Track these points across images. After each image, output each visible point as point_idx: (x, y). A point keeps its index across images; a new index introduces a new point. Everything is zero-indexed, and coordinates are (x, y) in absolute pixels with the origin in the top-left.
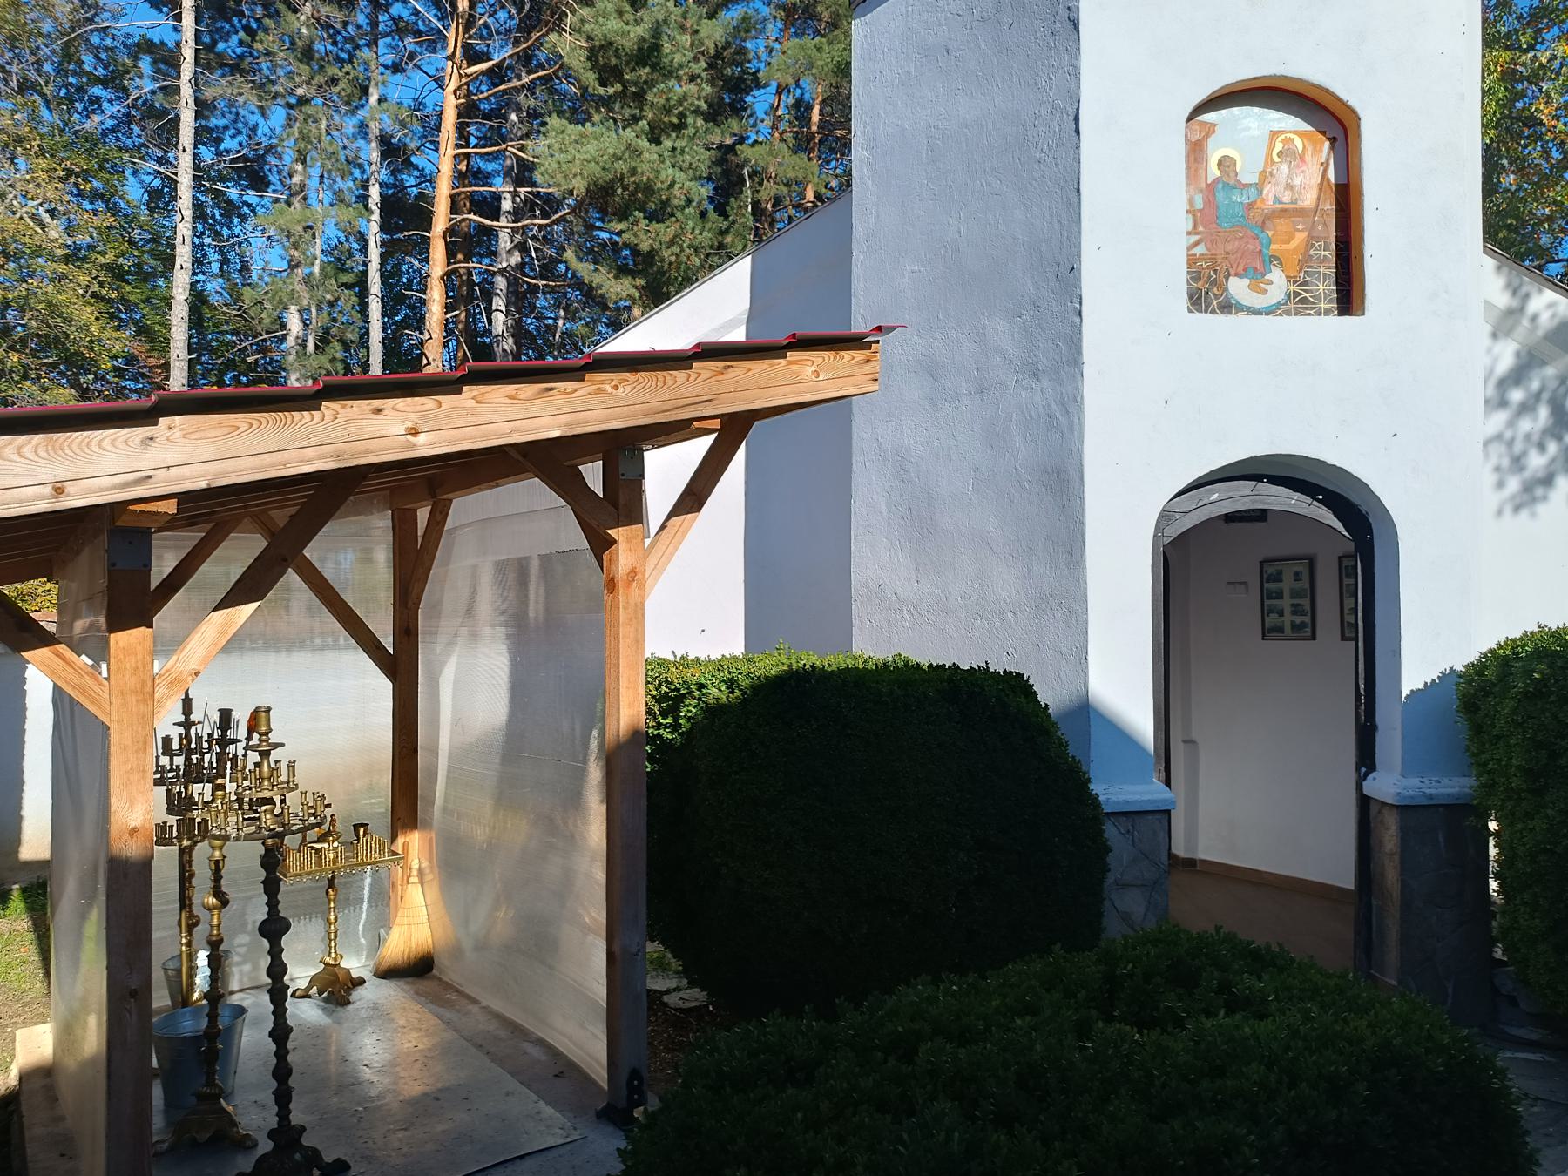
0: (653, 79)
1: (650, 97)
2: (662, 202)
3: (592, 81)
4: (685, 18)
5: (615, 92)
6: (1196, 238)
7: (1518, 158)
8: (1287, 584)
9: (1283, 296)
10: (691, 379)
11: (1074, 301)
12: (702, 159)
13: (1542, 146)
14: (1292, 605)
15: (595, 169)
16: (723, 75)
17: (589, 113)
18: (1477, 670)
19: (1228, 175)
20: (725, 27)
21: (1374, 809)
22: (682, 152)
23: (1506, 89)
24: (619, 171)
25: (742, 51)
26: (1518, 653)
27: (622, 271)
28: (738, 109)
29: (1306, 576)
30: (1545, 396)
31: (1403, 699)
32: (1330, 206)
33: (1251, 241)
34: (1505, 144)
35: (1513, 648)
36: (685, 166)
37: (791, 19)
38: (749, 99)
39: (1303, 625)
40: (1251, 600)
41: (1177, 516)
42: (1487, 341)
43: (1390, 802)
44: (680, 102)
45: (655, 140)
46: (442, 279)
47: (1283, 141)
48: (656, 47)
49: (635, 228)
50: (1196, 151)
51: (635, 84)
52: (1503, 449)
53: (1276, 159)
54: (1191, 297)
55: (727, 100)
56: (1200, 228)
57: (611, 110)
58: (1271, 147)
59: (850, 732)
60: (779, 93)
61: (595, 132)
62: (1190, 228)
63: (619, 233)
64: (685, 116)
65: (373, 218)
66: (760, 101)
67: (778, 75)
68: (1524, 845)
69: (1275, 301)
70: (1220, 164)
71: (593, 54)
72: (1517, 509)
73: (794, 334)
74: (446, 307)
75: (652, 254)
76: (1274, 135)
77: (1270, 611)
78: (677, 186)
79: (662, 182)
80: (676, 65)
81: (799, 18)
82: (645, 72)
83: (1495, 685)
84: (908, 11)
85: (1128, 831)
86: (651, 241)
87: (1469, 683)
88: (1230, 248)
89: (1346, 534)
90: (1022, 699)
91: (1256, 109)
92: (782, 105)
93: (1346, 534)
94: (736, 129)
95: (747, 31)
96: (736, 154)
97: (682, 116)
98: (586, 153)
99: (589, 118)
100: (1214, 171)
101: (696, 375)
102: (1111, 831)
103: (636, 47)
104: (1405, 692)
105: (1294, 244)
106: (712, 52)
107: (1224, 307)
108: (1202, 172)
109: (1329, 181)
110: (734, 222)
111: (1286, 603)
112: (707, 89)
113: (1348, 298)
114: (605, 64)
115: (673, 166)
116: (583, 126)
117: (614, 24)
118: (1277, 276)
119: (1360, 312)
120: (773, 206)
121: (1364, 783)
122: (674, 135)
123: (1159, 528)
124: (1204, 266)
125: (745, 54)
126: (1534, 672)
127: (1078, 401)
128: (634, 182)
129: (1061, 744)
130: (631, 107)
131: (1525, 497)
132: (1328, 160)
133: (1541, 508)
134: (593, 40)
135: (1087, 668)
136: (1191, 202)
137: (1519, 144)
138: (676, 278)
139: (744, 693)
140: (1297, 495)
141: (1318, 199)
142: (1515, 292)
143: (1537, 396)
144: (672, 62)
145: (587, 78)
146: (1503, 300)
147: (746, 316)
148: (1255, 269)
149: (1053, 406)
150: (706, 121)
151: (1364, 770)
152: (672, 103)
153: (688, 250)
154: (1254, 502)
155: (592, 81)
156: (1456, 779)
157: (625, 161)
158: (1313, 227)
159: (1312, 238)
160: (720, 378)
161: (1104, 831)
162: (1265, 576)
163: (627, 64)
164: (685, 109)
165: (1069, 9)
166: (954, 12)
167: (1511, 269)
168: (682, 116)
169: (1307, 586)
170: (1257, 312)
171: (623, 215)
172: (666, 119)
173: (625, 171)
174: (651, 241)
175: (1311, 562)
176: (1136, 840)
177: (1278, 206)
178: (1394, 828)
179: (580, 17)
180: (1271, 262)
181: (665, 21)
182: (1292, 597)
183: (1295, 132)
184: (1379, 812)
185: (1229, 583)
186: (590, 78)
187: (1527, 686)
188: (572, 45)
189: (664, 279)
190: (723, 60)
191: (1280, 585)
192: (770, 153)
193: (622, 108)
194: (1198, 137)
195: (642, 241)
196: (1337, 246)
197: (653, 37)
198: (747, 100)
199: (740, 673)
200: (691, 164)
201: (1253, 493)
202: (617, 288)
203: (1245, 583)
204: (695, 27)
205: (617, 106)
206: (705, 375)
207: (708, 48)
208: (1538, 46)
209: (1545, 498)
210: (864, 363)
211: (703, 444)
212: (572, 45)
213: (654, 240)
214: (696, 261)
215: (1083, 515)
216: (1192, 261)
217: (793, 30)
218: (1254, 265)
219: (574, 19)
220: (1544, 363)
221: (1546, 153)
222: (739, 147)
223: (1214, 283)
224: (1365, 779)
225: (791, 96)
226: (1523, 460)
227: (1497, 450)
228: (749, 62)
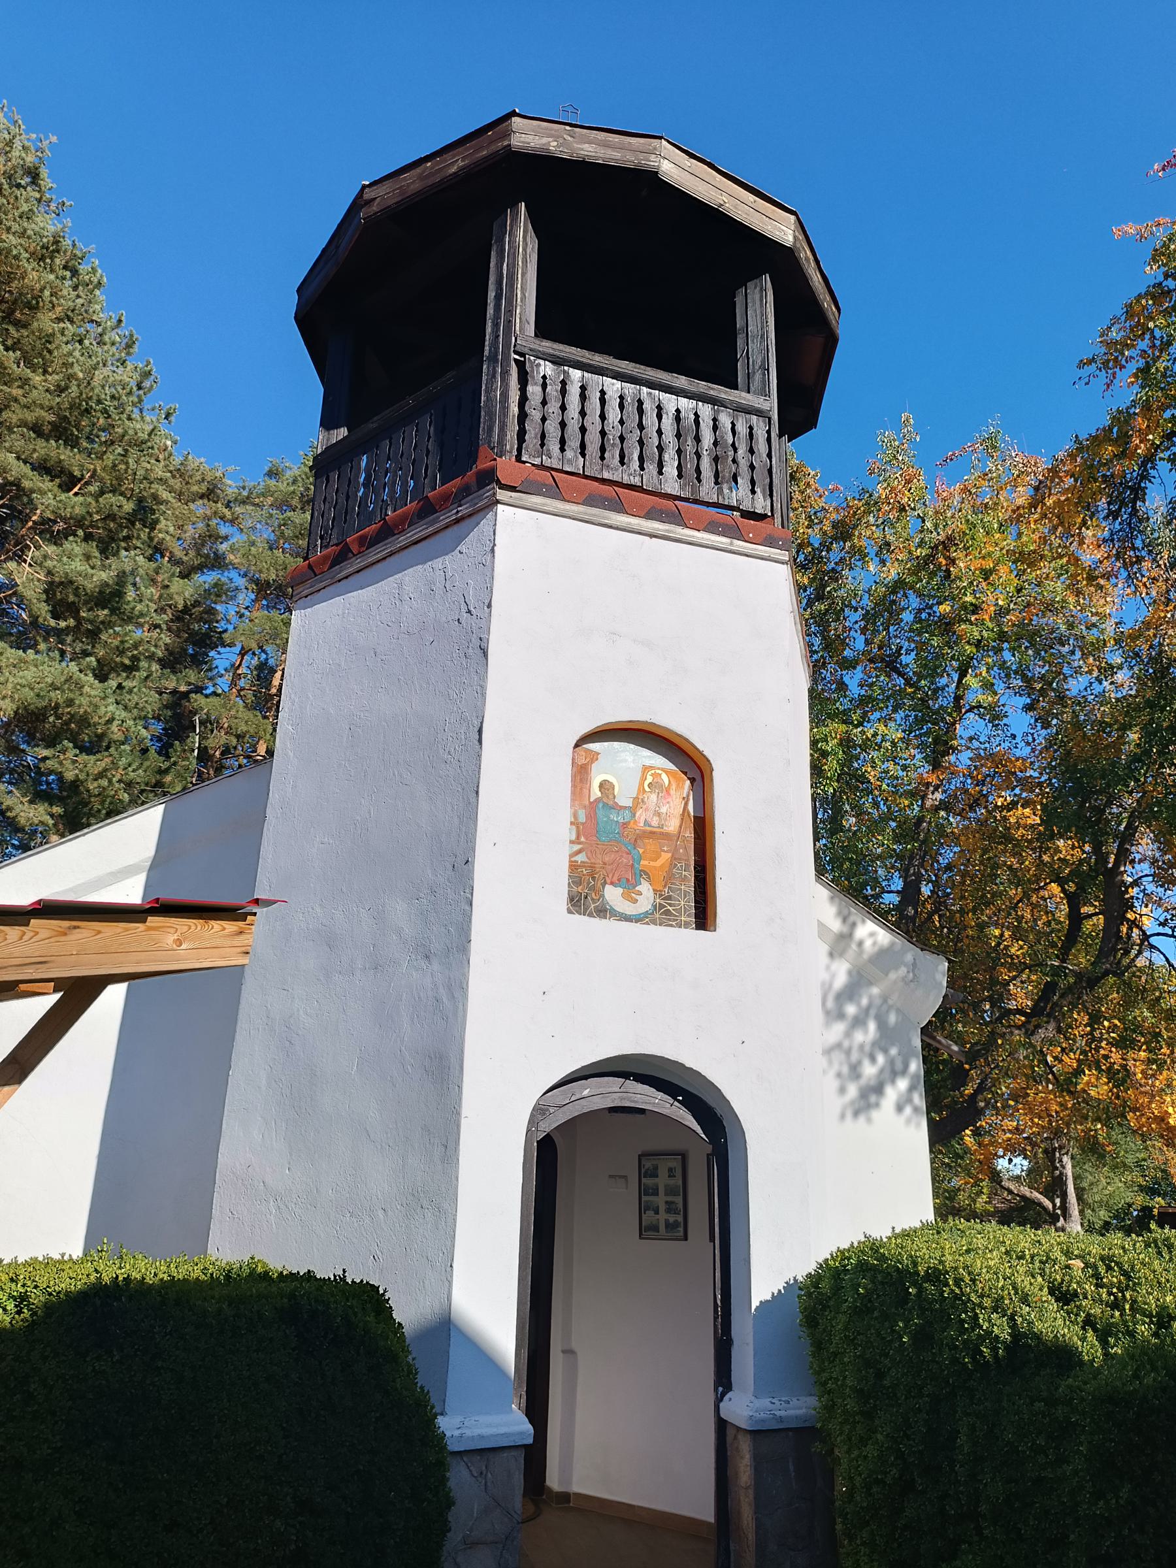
0: (110, 621)
1: (104, 637)
2: (97, 736)
3: (43, 613)
4: (157, 573)
5: (68, 627)
6: (579, 847)
7: (856, 806)
8: (662, 1181)
9: (650, 907)
10: (26, 938)
11: (467, 891)
12: (151, 701)
13: (873, 799)
14: (667, 1202)
15: (29, 695)
16: (189, 629)
17: (36, 641)
18: (814, 1280)
19: (608, 797)
20: (197, 588)
21: (730, 1433)
22: (130, 691)
23: (843, 751)
24: (54, 700)
25: (211, 611)
26: (845, 1266)
27: (39, 796)
28: (198, 661)
29: (679, 1173)
30: (873, 1012)
31: (753, 1310)
32: (689, 834)
33: (624, 855)
34: (846, 793)
35: (842, 1260)
36: (131, 704)
37: (263, 593)
38: (212, 654)
39: (675, 1225)
40: (630, 1193)
41: (552, 1110)
42: (824, 959)
43: (743, 1426)
44: (136, 646)
45: (102, 677)
47: (652, 775)
48: (119, 594)
49: (62, 757)
50: (581, 773)
51: (91, 622)
52: (843, 1056)
53: (647, 789)
54: (571, 899)
55: (191, 651)
56: (583, 839)
57: (62, 642)
58: (644, 779)
59: (160, 1364)
60: (243, 654)
61: (37, 660)
62: (574, 838)
63: (45, 759)
64: (139, 660)
66: (222, 658)
67: (243, 638)
68: (860, 1475)
69: (643, 910)
70: (601, 786)
71: (50, 590)
72: (856, 1114)
73: (158, 899)
75: (75, 785)
76: (646, 769)
77: (647, 1208)
78: (116, 723)
79: (100, 717)
80: (137, 613)
81: (271, 593)
82: (103, 613)
83: (830, 1298)
84: (344, 613)
85: (481, 1473)
86: (77, 771)
87: (809, 1295)
88: (607, 859)
89: (703, 1136)
90: (371, 1318)
91: (632, 746)
92: (244, 664)
93: (703, 1136)
94: (193, 679)
95: (218, 596)
96: (189, 701)
97: (135, 659)
98: (21, 678)
99: (34, 646)
100: (596, 793)
101: (32, 934)
102: (460, 1479)
103: (97, 590)
104: (755, 1304)
105: (658, 863)
106: (180, 607)
107: (601, 911)
108: (586, 791)
110: (175, 764)
111: (661, 1200)
112: (167, 639)
113: (704, 917)
114: (61, 600)
115: (117, 703)
116: (24, 652)
117: (78, 565)
118: (645, 889)
119: (712, 928)
120: (222, 754)
121: (721, 1405)
122: (124, 674)
123: (533, 1121)
124: (585, 872)
125: (214, 614)
126: (860, 1287)
127: (463, 988)
128: (69, 713)
129: (410, 1372)
130: (83, 642)
132: (688, 796)
133: (875, 1114)
134: (53, 575)
135: (452, 1276)
136: (575, 815)
137: (856, 795)
138: (99, 811)
139: (34, 1314)
140: (660, 1095)
141: (680, 827)
142: (845, 920)
144: (133, 609)
145: (39, 609)
146: (836, 925)
147: (149, 863)
148: (628, 880)
149: (441, 990)
150: (163, 667)
151: (721, 1389)
152: (127, 645)
153: (117, 785)
154: (622, 1099)
155: (43, 613)
156: (803, 1399)
157: (63, 691)
158: (676, 849)
159: (675, 859)
160: (63, 938)
161: (448, 1479)
162: (643, 1171)
163: (86, 603)
164: (140, 653)
165: (481, 639)
166: (385, 623)
167: (841, 900)
168: (135, 659)
169: (680, 1183)
170: (627, 918)
171: (51, 742)
172: (118, 659)
173: (61, 701)
174: (77, 771)
175: (684, 1156)
176: (489, 1484)
177: (649, 829)
178: (748, 1456)
179: (43, 553)
181: (132, 573)
182: (666, 1194)
183: (663, 770)
184: (735, 1438)
185: (611, 1176)
186: (43, 610)
187: (855, 1301)
188: (30, 576)
189: (86, 810)
190: (191, 615)
191: (656, 1180)
192: (224, 706)
193: (74, 641)
194: (583, 762)
195: (67, 769)
196: (695, 868)
197: (117, 584)
198: (210, 654)
199: (36, 1287)
200: (137, 704)
201: (621, 1090)
202: (30, 813)
203: (625, 1177)
204: (166, 582)
205: (69, 639)
206: (43, 934)
207: (176, 603)
208: (865, 724)
210: (237, 935)
211: (44, 1003)
212: (30, 576)
213: (81, 771)
214: (126, 797)
215: (460, 1106)
216: (573, 867)
217: (264, 602)
219: (37, 553)
220: (870, 984)
221: (876, 805)
222: (193, 695)
223: (593, 888)
224: (721, 1400)
225: (256, 658)
227: (838, 1056)
228: (217, 622)
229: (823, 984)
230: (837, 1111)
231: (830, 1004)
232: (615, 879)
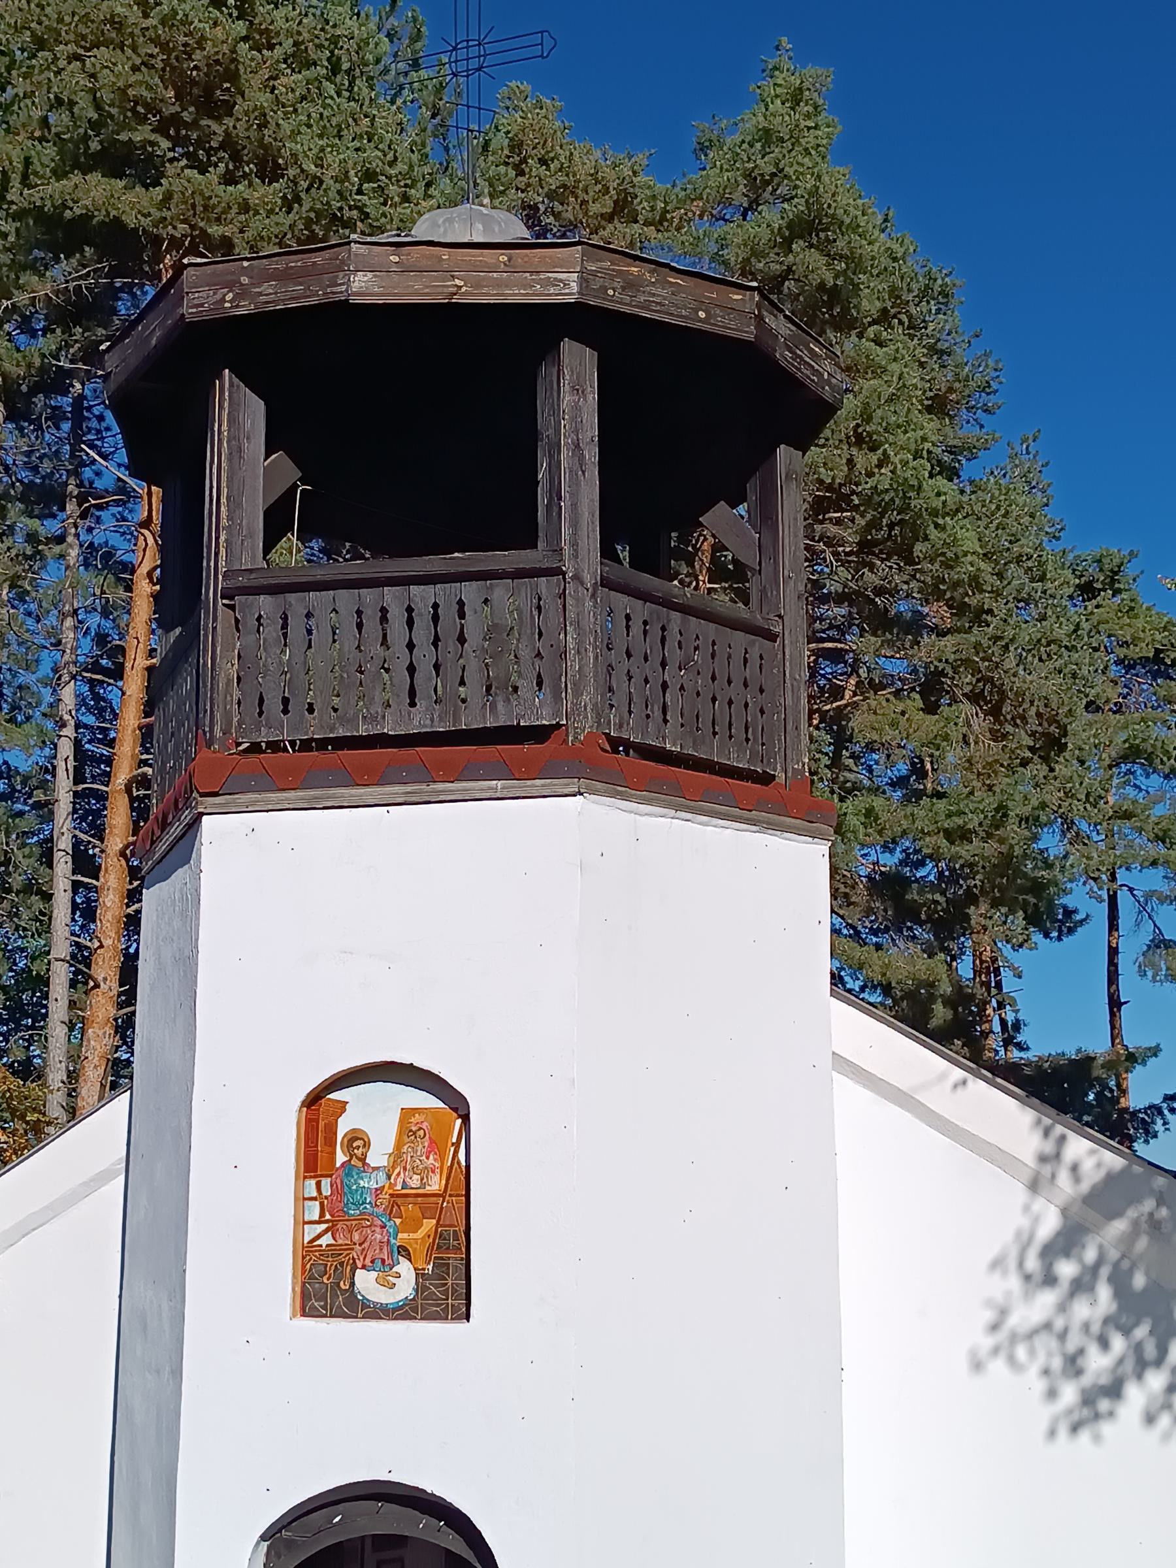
6: (324, 1226)
9: (410, 1291)
30: (1105, 1271)
46: (122, 854)
52: (1054, 1344)
56: (328, 1217)
65: (64, 732)
72: (1075, 1428)
74: (128, 897)
109: (459, 1163)
131: (1086, 1412)
142: (1047, 1133)
143: (1095, 1269)
180: (399, 1252)
209: (1111, 1414)
218: (382, 1256)
220: (1096, 1229)
226: (1079, 1361)
229: (1018, 1234)
230: (1043, 1425)
231: (1033, 1263)
232: (368, 1262)
